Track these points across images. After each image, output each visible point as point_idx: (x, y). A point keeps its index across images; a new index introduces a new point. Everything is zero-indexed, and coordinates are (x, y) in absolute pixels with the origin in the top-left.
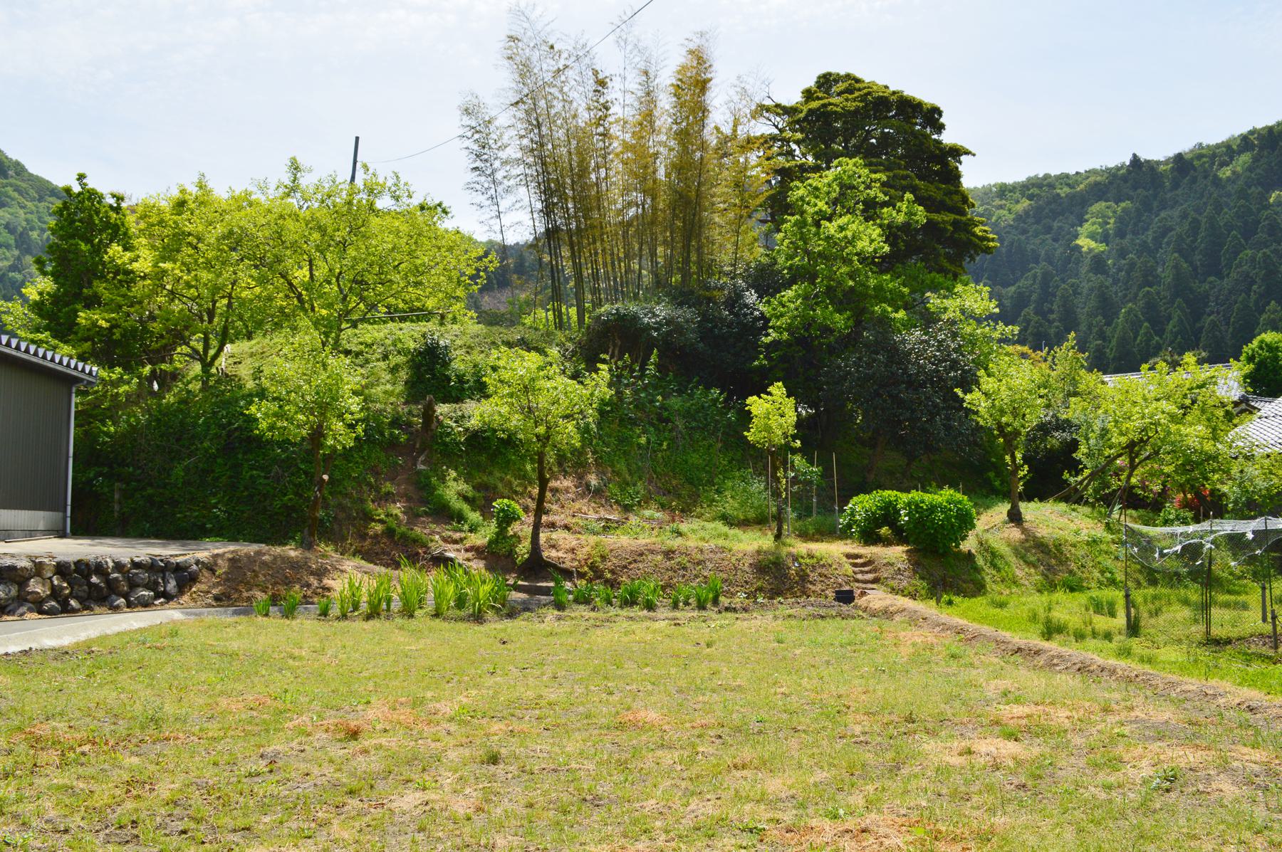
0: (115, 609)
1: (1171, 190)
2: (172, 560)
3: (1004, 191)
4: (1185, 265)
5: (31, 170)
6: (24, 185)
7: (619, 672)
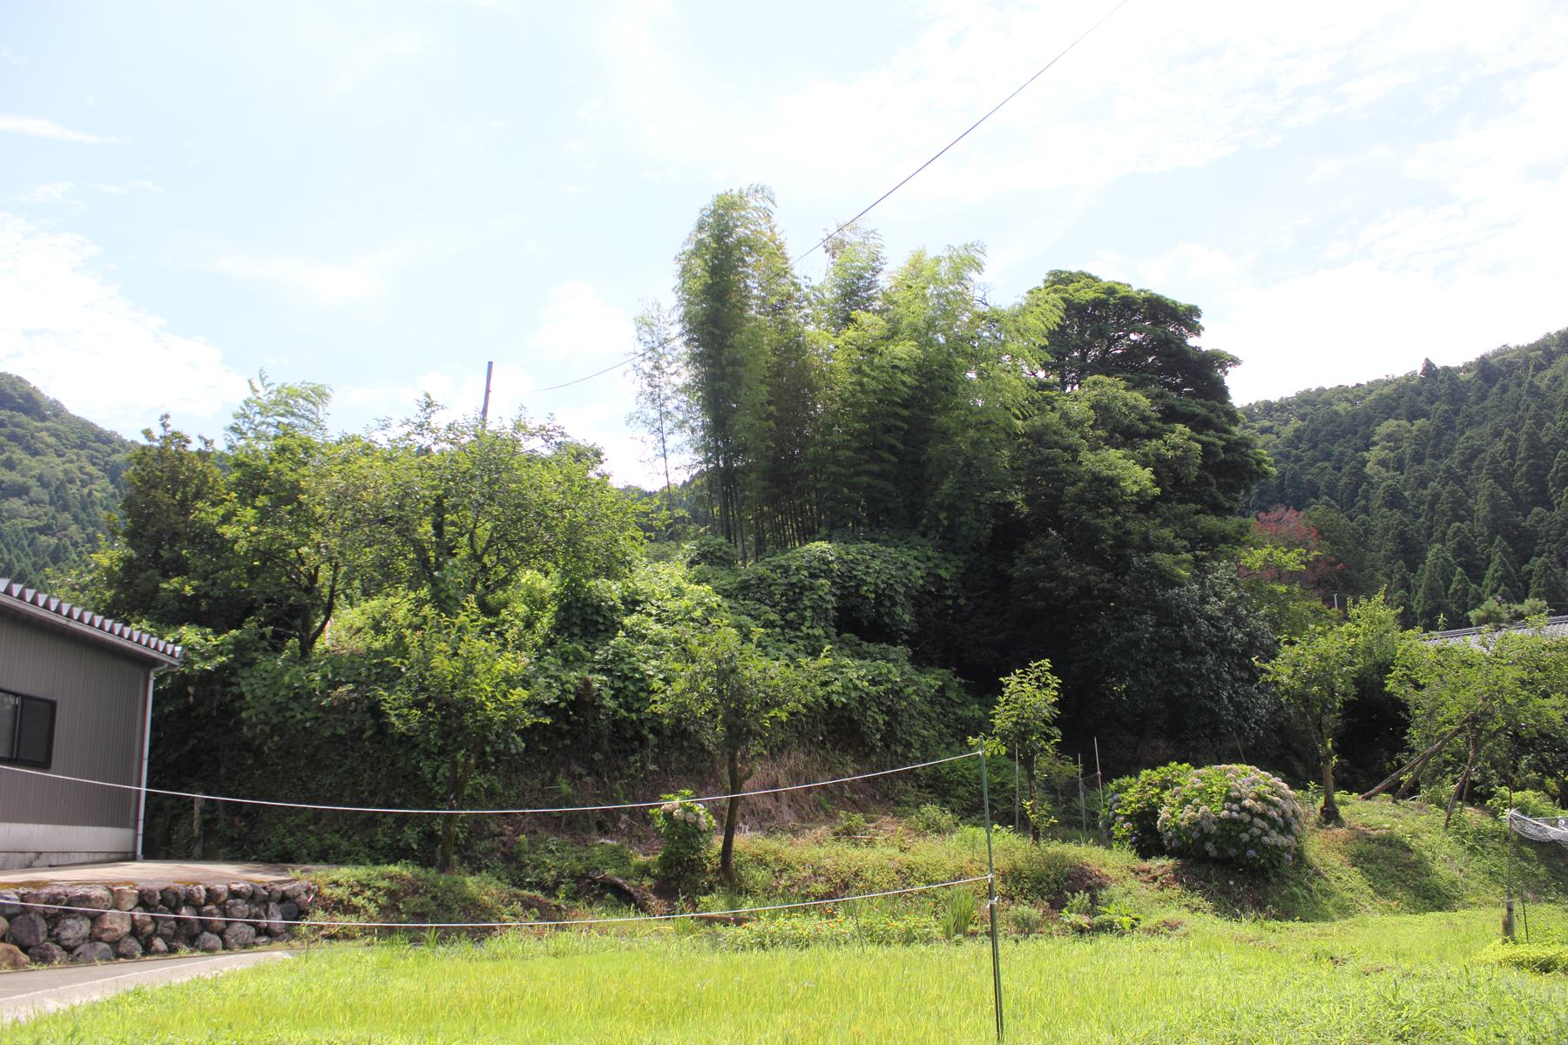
0: (210, 951)
1: (1475, 403)
2: (277, 887)
3: (1268, 408)
4: (1503, 494)
5: (78, 407)
6: (62, 428)
7: (1096, 920)
